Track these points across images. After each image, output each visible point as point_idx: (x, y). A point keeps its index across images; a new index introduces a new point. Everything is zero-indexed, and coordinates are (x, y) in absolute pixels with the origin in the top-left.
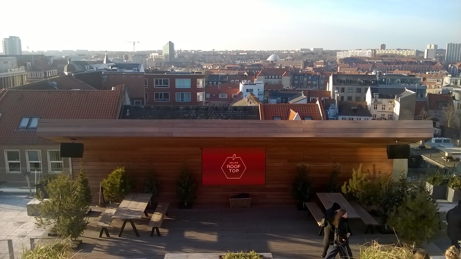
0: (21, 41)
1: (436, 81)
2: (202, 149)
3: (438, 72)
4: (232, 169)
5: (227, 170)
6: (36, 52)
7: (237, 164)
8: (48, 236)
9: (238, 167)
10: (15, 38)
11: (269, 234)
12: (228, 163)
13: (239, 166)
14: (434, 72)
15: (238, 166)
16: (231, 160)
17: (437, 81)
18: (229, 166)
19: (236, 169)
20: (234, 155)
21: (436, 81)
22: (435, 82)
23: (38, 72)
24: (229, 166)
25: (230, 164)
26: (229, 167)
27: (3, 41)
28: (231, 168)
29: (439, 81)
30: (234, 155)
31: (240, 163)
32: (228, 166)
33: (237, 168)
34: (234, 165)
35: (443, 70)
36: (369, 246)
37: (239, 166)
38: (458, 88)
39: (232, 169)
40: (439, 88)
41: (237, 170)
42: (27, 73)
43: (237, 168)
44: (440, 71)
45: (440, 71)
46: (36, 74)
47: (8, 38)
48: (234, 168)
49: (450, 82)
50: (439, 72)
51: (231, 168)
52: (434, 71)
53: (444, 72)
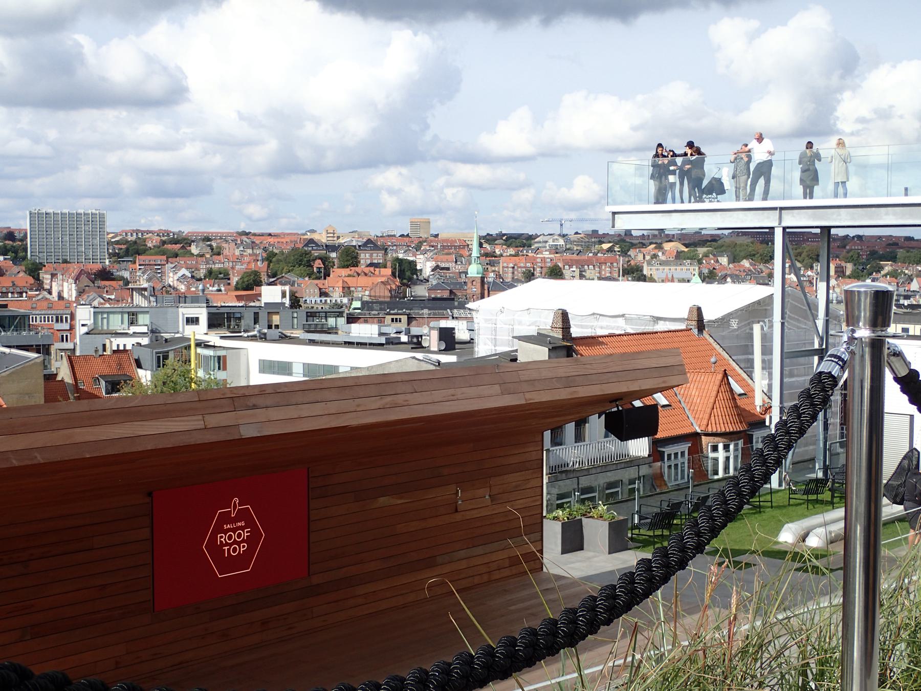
1: (52, 321)
2: (150, 494)
3: (22, 297)
4: (231, 545)
5: (218, 551)
7: (242, 528)
8: (908, 329)
9: (246, 535)
11: (867, 355)
12: (219, 529)
13: (247, 532)
14: (8, 297)
15: (245, 534)
16: (226, 518)
17: (57, 321)
18: (222, 538)
19: (239, 543)
20: (235, 502)
21: (52, 321)
22: (50, 322)
24: (222, 538)
25: (225, 532)
26: (222, 540)
28: (227, 544)
29: (62, 321)
30: (235, 502)
31: (250, 524)
32: (221, 537)
33: (243, 541)
34: (234, 530)
35: (36, 290)
36: (662, 600)
37: (247, 532)
38: (120, 335)
39: (231, 545)
40: (63, 341)
41: (244, 547)
42: (129, 329)
43: (243, 541)
44: (26, 293)
45: (26, 293)
48: (235, 542)
49: (92, 321)
50: (24, 295)
51: (227, 544)
52: (10, 295)
53: (37, 295)
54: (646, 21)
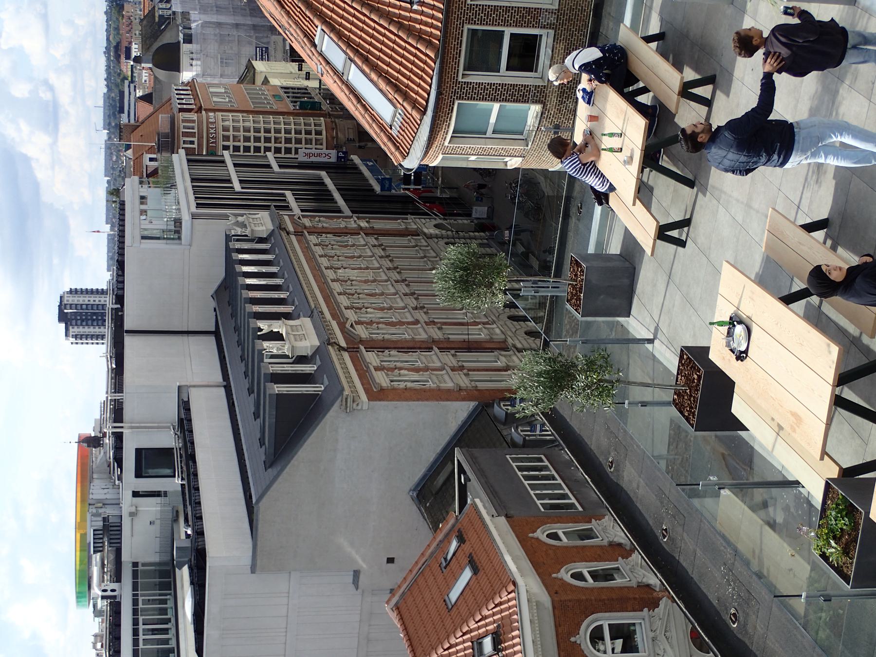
0: (73, 288)
6: (108, 182)
10: (65, 305)
23: (179, 128)
27: (73, 340)
46: (185, 134)
47: (63, 325)
54: (213, 304)
